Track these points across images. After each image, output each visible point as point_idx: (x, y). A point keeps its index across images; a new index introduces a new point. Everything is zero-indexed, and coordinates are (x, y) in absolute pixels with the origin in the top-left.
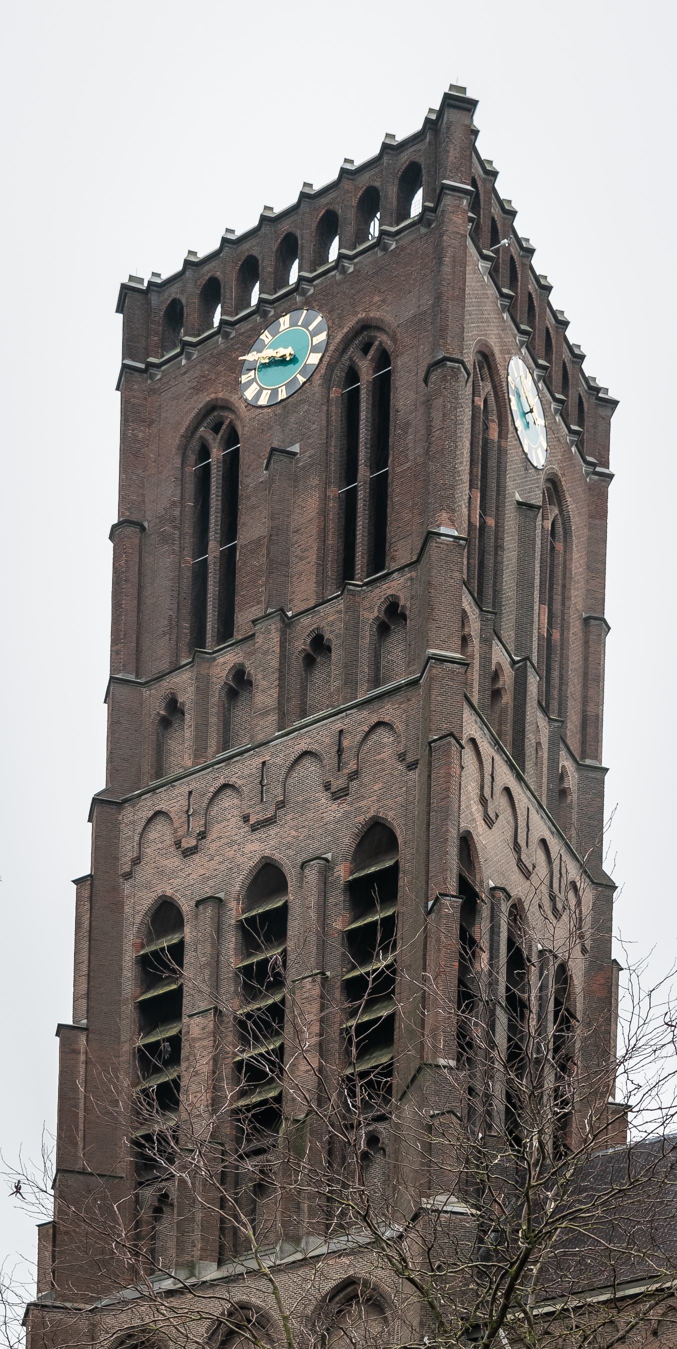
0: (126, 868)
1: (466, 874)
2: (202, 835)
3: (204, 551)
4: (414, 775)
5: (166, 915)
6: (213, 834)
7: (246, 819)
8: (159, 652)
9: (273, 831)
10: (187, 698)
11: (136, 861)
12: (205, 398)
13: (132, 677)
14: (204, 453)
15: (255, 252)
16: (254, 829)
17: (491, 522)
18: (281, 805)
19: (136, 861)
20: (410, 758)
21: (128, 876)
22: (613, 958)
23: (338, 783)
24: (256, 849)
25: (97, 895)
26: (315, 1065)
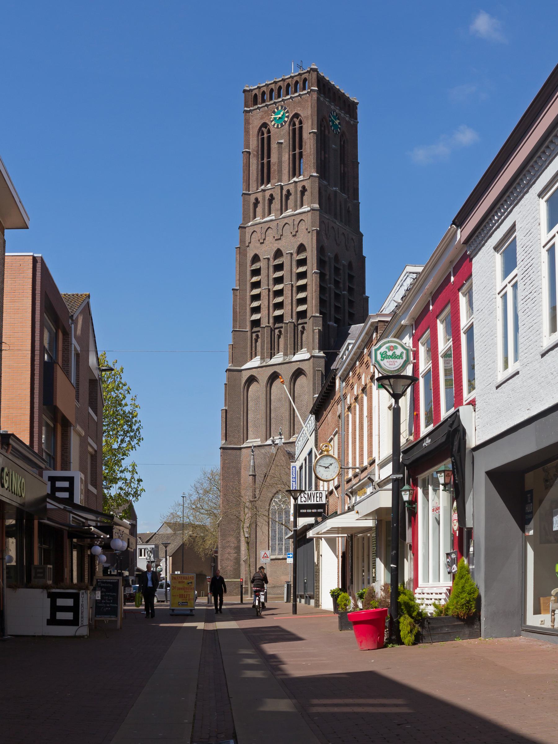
0: (247, 244)
1: (322, 258)
2: (264, 239)
3: (263, 160)
4: (310, 234)
5: (256, 259)
6: (267, 239)
7: (274, 237)
9: (280, 241)
10: (260, 199)
11: (250, 243)
12: (263, 121)
13: (247, 192)
14: (263, 134)
15: (273, 88)
16: (276, 240)
17: (327, 156)
18: (282, 235)
19: (250, 243)
20: (309, 230)
21: (248, 246)
22: (49, 599)
23: (294, 233)
24: (276, 246)
26: (330, 489)
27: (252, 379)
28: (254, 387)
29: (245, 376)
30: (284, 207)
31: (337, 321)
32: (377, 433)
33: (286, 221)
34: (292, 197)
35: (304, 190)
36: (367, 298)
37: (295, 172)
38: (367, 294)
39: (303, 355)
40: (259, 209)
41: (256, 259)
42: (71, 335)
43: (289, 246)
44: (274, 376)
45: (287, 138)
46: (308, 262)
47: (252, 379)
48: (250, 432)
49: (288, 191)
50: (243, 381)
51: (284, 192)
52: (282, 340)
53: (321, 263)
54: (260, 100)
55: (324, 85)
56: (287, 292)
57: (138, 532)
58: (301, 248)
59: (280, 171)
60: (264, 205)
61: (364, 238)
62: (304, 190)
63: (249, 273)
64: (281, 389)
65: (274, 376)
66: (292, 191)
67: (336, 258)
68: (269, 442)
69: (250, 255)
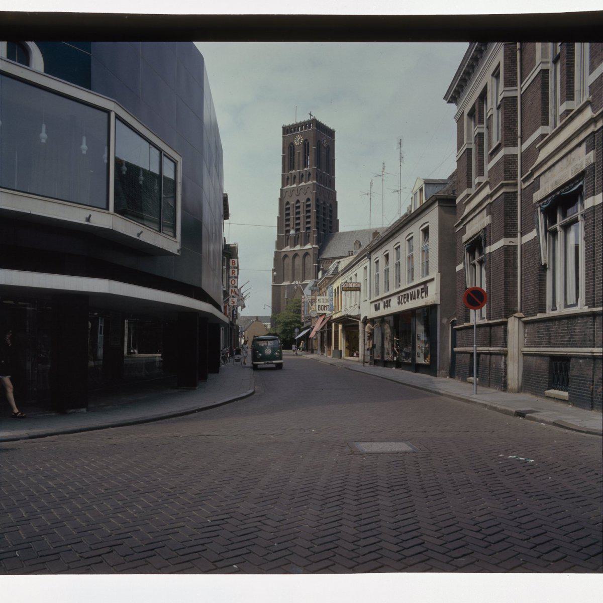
5: (288, 203)
8: (286, 171)
25: (281, 200)
27: (286, 256)
28: (287, 260)
29: (283, 255)
30: (300, 182)
31: (324, 231)
32: (150, 552)
33: (301, 187)
34: (290, 180)
35: (310, 174)
36: (338, 220)
37: (305, 165)
38: (338, 218)
39: (309, 246)
40: (289, 182)
41: (288, 203)
42: (502, 125)
43: (303, 200)
44: (296, 255)
45: (302, 150)
46: (311, 205)
47: (286, 256)
48: (285, 279)
49: (302, 174)
50: (282, 257)
51: (301, 175)
52: (300, 240)
53: (317, 206)
54: (289, 131)
55: (327, 130)
56: (302, 219)
57: (536, 43)
58: (308, 200)
59: (299, 165)
60: (306, 176)
61: (337, 194)
62: (310, 174)
63: (284, 210)
64: (298, 261)
65: (296, 255)
66: (304, 174)
67: (324, 203)
68: (293, 283)
69: (285, 202)
